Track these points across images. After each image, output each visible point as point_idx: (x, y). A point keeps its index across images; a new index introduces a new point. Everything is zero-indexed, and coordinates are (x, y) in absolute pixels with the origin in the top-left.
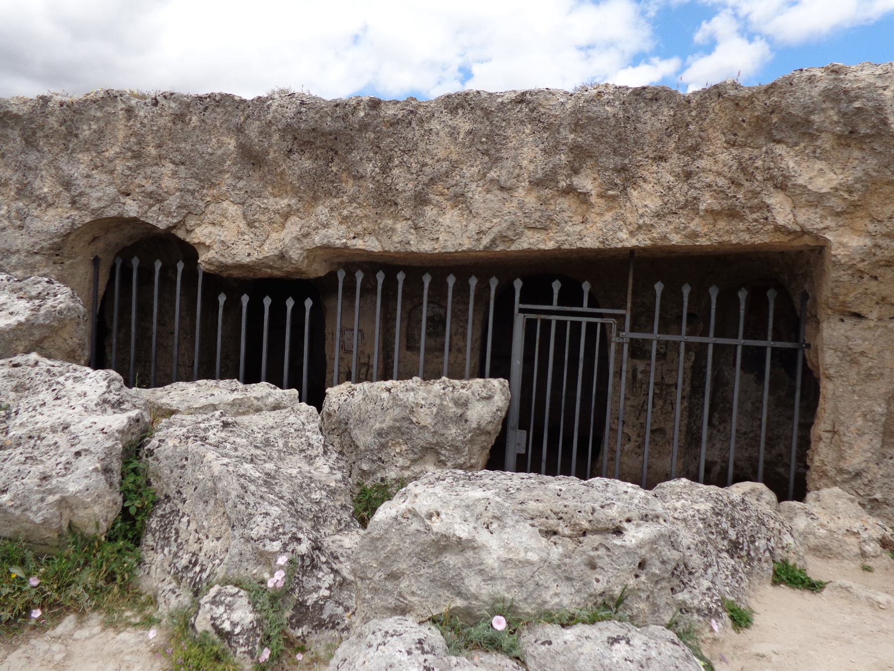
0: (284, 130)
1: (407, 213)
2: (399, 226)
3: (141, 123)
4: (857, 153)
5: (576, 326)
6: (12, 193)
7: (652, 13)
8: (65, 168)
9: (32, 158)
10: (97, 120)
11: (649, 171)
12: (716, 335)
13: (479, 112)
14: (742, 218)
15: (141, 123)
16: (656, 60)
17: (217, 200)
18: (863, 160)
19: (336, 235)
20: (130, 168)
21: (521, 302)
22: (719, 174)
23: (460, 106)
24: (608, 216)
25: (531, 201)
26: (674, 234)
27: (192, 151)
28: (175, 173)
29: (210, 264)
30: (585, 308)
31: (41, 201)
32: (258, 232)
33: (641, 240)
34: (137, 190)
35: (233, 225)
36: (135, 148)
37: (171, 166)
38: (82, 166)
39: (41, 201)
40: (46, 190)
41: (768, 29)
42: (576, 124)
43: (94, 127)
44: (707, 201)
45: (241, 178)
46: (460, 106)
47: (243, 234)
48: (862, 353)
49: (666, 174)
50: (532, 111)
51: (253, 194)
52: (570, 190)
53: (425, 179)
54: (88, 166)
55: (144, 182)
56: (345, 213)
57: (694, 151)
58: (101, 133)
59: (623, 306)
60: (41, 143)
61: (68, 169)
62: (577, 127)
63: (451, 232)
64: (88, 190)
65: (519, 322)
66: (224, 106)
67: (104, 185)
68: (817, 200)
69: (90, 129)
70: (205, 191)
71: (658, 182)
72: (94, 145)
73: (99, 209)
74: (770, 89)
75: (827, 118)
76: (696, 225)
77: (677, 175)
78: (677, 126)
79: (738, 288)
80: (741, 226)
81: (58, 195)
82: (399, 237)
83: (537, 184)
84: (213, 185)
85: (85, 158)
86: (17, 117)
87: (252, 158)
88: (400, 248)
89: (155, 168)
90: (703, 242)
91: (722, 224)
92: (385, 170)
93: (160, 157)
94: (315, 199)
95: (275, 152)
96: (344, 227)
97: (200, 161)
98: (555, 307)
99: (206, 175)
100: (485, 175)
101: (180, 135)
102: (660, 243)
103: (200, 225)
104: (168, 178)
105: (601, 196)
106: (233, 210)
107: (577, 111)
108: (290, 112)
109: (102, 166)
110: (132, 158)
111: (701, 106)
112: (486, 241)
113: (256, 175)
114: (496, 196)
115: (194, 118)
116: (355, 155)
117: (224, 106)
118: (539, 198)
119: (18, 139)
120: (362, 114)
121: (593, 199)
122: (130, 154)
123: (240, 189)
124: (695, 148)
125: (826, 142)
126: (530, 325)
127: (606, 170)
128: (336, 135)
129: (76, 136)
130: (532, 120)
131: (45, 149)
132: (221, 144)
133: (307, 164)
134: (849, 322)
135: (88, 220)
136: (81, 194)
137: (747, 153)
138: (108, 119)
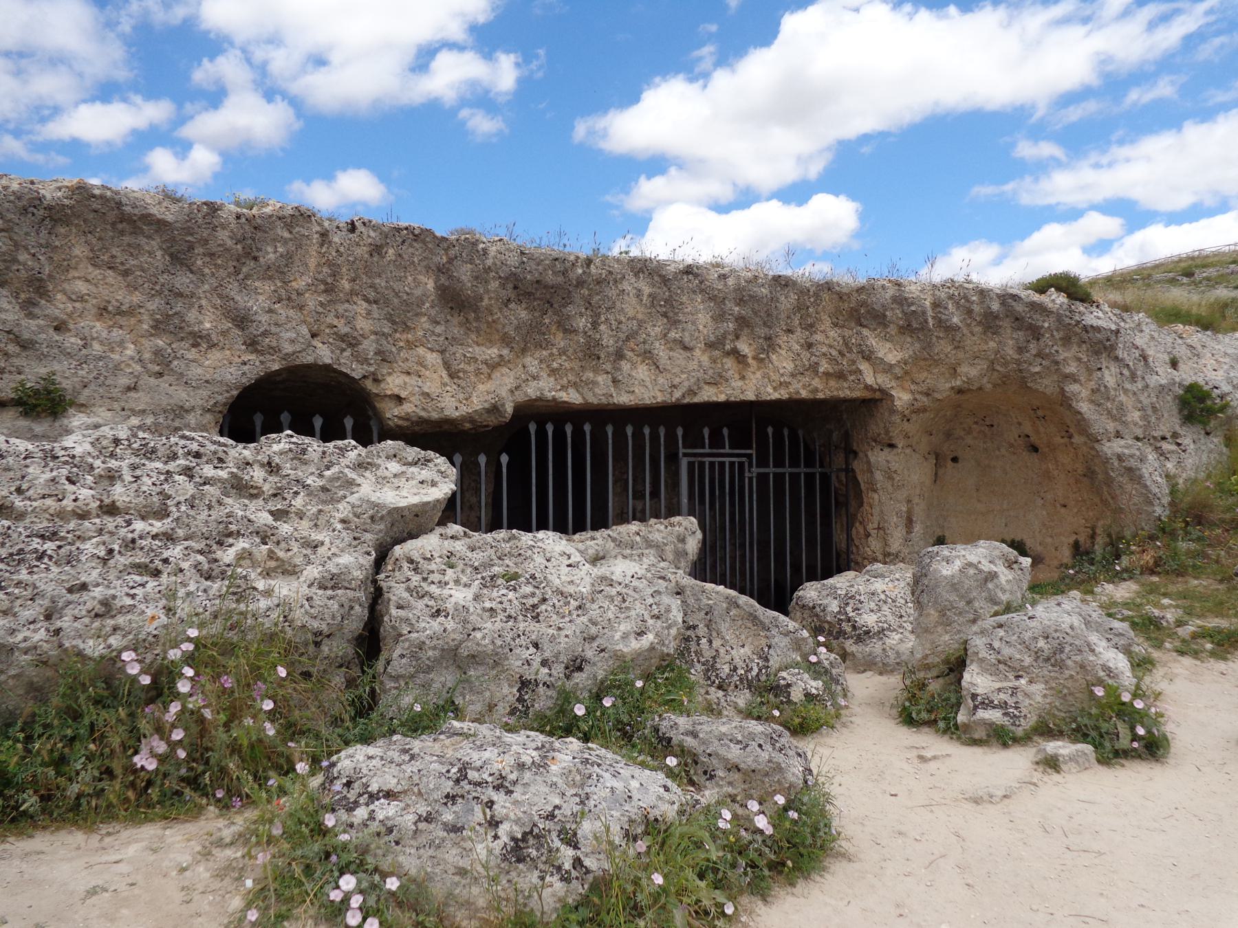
0: (507, 278)
1: (608, 367)
2: (600, 379)
3: (338, 251)
4: (909, 339)
5: (722, 464)
6: (145, 327)
7: (126, 26)
8: (238, 298)
9: (183, 280)
10: (285, 242)
11: (783, 339)
12: (806, 466)
13: (656, 278)
14: (846, 379)
15: (338, 251)
16: (138, 99)
17: (411, 345)
18: (912, 344)
19: (545, 388)
20: (321, 304)
21: (684, 447)
22: (831, 347)
23: (641, 270)
24: (759, 375)
25: (705, 359)
26: (802, 389)
27: (386, 288)
28: (369, 313)
29: (407, 420)
30: (727, 450)
31: (198, 339)
32: (463, 384)
33: (782, 394)
34: (327, 331)
35: (435, 376)
36: (329, 280)
37: (365, 305)
38: (261, 298)
39: (198, 339)
40: (208, 325)
41: (295, 88)
42: (741, 300)
43: (280, 250)
44: (824, 366)
45: (438, 323)
46: (641, 270)
47: (445, 385)
48: (895, 472)
49: (794, 342)
50: (701, 283)
51: (454, 341)
52: (735, 353)
53: (623, 336)
54: (269, 298)
55: (335, 322)
56: (555, 365)
57: (810, 327)
58: (289, 257)
59: (750, 448)
60: (199, 262)
61: (242, 300)
62: (741, 302)
63: (643, 386)
64: (273, 329)
65: (684, 463)
66: (424, 242)
67: (294, 324)
68: (889, 369)
69: (275, 252)
70: (398, 335)
71: (790, 349)
72: (277, 272)
73: (294, 353)
74: (860, 290)
75: (894, 314)
76: (816, 383)
77: (802, 346)
78: (800, 307)
79: (605, 424)
80: (846, 385)
81: (224, 333)
82: (601, 390)
83: (710, 346)
84: (407, 329)
85: (267, 287)
86: (161, 225)
87: (455, 301)
88: (604, 401)
89: (347, 305)
90: (821, 396)
91: (832, 383)
92: (595, 325)
93: (353, 293)
94: (524, 351)
95: (490, 299)
96: (552, 379)
97: (396, 301)
98: (707, 450)
99: (400, 318)
100: (665, 335)
101: (376, 270)
102: (795, 396)
103: (390, 374)
104: (363, 318)
105: (754, 358)
106: (433, 358)
107: (739, 289)
108: (513, 260)
109: (289, 299)
110: (325, 291)
111: (816, 295)
112: (678, 394)
113: (455, 321)
114: (679, 354)
115: (391, 251)
116: (571, 310)
117: (424, 242)
118: (710, 358)
119: (159, 253)
120: (580, 271)
121: (750, 361)
122: (322, 287)
123: (439, 335)
124: (812, 326)
125: (892, 329)
126: (691, 465)
127: (760, 337)
128: (555, 288)
129: (255, 259)
130: (702, 291)
131: (207, 271)
132: (418, 283)
133: (524, 314)
134: (887, 450)
135: (276, 367)
136: (266, 334)
137: (847, 333)
138: (299, 242)
